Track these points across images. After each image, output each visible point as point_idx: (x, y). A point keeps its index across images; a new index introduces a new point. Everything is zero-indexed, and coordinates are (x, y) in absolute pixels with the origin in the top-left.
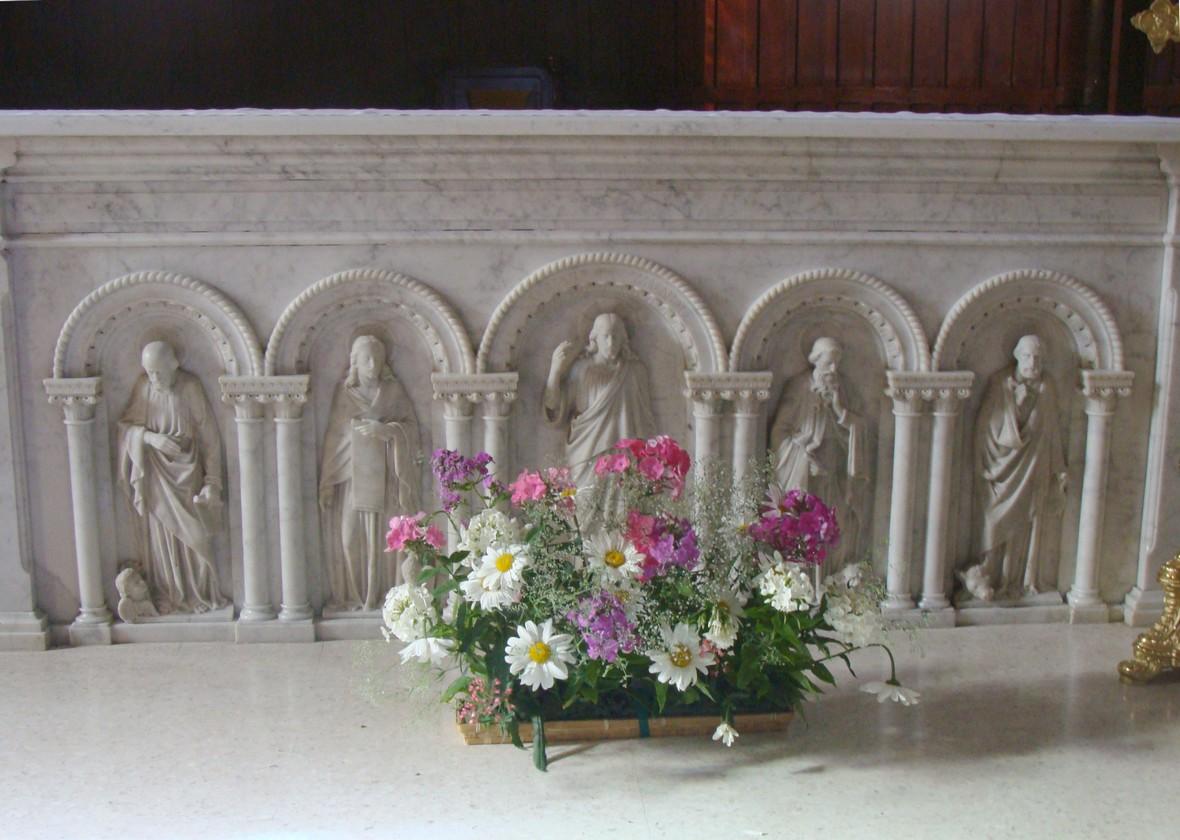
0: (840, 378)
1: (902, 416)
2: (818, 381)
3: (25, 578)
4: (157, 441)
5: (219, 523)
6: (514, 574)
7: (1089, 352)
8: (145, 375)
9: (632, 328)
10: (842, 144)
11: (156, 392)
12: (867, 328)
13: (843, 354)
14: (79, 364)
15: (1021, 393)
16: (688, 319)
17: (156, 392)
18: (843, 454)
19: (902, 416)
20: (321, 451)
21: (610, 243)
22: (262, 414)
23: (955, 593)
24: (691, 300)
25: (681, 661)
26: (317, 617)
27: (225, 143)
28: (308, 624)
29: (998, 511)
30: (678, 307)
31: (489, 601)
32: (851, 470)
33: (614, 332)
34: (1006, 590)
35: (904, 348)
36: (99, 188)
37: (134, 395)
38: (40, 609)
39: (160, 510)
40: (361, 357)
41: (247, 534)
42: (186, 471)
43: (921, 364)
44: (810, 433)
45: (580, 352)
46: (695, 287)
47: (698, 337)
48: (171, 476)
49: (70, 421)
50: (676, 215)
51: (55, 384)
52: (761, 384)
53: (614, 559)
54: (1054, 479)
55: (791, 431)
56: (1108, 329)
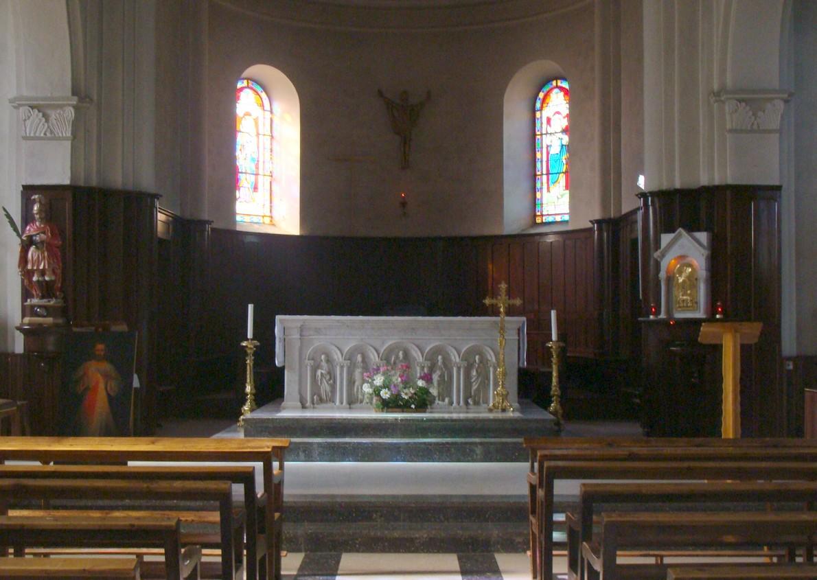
0: (444, 363)
1: (455, 370)
2: (440, 363)
3: (299, 396)
4: (323, 372)
5: (333, 387)
6: (382, 380)
7: (490, 358)
8: (321, 360)
9: (407, 354)
10: (441, 321)
11: (324, 364)
12: (448, 354)
13: (444, 359)
14: (311, 358)
15: (477, 365)
16: (416, 352)
17: (324, 364)
18: (444, 376)
19: (455, 370)
20: (351, 375)
21: (402, 339)
22: (342, 367)
23: (467, 403)
24: (416, 349)
25: (406, 394)
26: (350, 404)
27: (338, 321)
28: (348, 406)
29: (475, 387)
30: (414, 350)
31: (378, 384)
32: (446, 379)
33: (403, 354)
34: (476, 403)
35: (455, 358)
36: (316, 328)
37: (320, 363)
38: (301, 402)
39: (323, 384)
40: (359, 358)
41: (338, 389)
42: (328, 377)
43: (458, 360)
44: (438, 373)
45: (397, 357)
46: (418, 346)
47: (418, 355)
48: (325, 378)
49: (309, 368)
50: (414, 334)
51: (307, 361)
52: (429, 363)
53: (397, 380)
54: (485, 383)
55: (435, 372)
56: (492, 354)
